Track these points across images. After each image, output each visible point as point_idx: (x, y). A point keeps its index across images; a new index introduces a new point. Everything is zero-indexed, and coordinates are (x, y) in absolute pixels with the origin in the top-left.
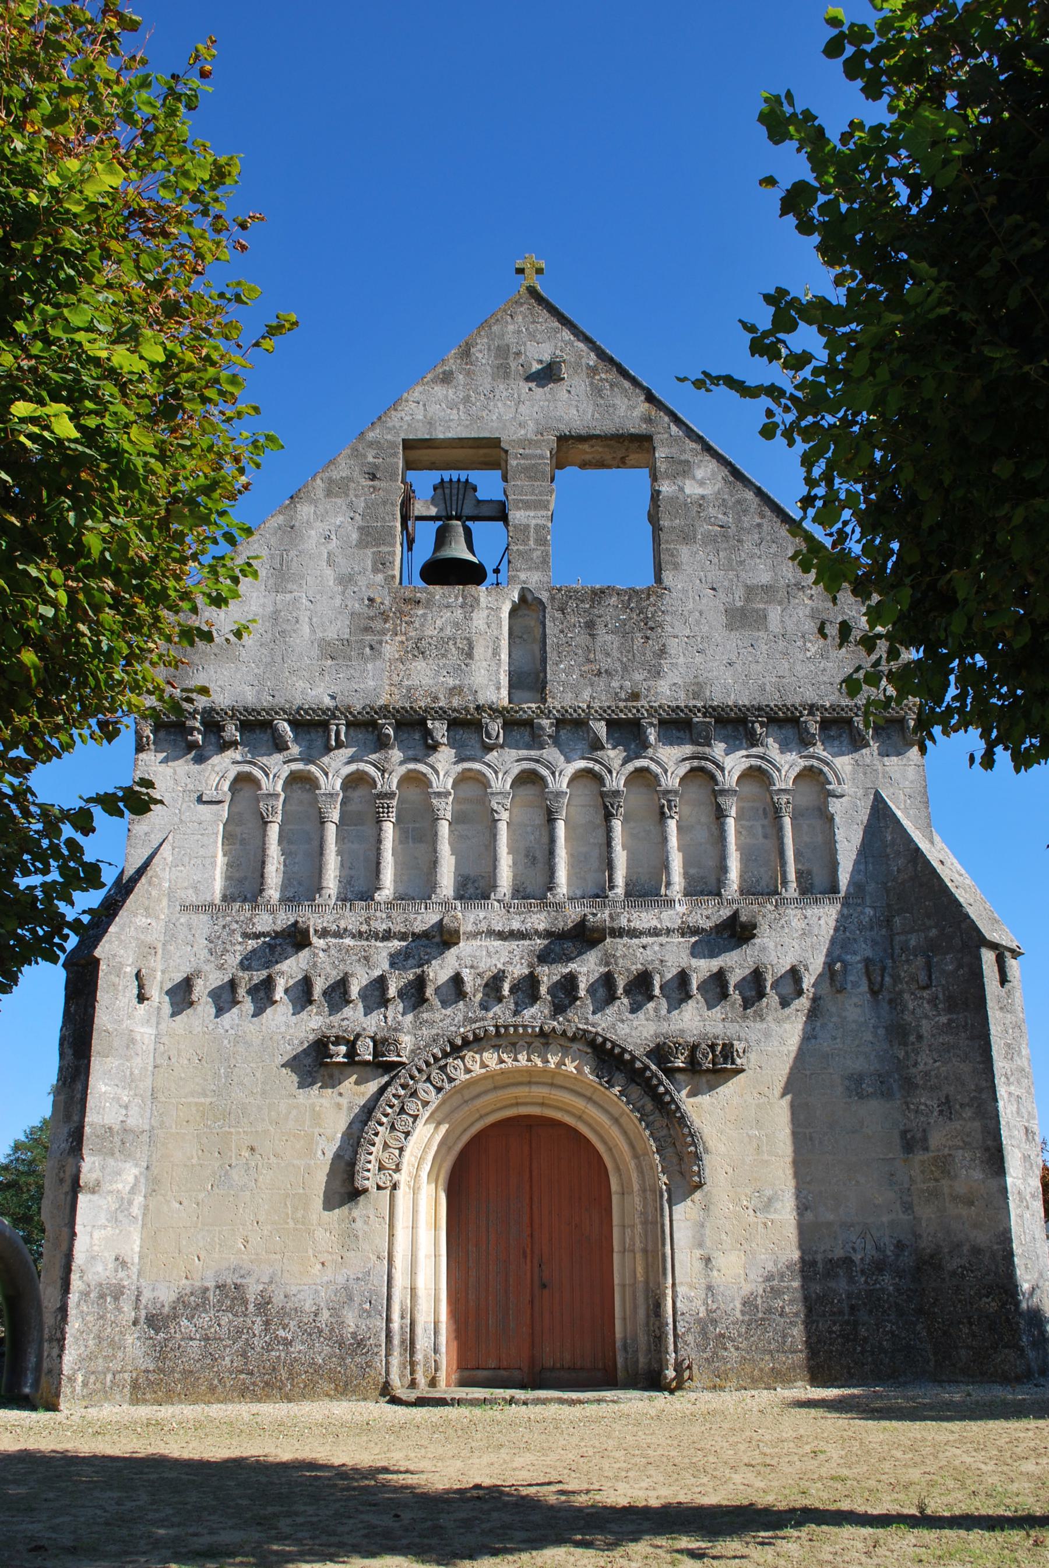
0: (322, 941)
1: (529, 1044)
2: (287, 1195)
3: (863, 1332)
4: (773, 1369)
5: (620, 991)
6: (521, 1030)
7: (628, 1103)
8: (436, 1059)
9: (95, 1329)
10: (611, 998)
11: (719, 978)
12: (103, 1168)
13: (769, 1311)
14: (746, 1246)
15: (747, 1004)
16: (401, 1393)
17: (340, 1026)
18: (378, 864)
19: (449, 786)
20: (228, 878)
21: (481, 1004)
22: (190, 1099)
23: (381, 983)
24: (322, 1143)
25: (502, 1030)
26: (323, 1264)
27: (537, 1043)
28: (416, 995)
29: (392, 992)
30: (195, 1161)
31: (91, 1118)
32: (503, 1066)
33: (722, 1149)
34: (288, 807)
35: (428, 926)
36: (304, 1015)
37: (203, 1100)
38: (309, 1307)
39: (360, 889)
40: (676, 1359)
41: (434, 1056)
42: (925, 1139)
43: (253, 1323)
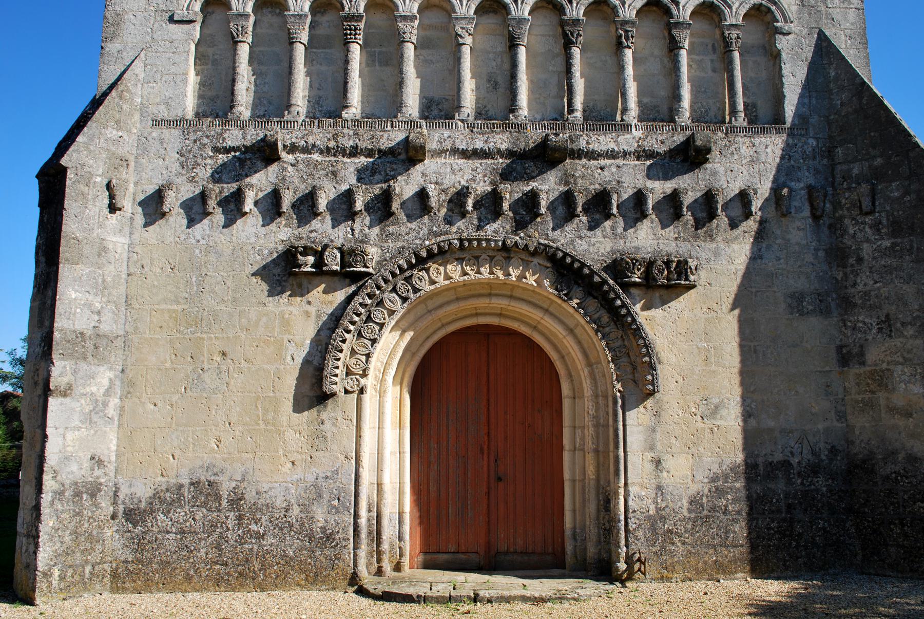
0: (290, 156)
1: (492, 258)
2: (258, 398)
3: (798, 529)
4: (716, 561)
5: (579, 209)
6: (484, 244)
7: (586, 315)
8: (402, 270)
9: (71, 526)
10: (571, 215)
11: (674, 199)
12: (75, 372)
13: (713, 509)
14: (693, 450)
15: (698, 225)
16: (367, 579)
17: (309, 238)
18: (346, 83)
19: (415, 11)
20: (201, 97)
21: (445, 219)
22: (163, 306)
23: (348, 197)
24: (292, 349)
25: (466, 244)
26: (293, 463)
27: (499, 257)
28: (382, 208)
29: (359, 205)
30: (168, 365)
31: (60, 323)
32: (466, 278)
33: (673, 360)
34: (258, 30)
35: (394, 143)
36: (273, 226)
37: (175, 307)
38: (279, 503)
39: (329, 106)
40: (627, 553)
41: (400, 267)
42: (862, 354)
43: (227, 517)
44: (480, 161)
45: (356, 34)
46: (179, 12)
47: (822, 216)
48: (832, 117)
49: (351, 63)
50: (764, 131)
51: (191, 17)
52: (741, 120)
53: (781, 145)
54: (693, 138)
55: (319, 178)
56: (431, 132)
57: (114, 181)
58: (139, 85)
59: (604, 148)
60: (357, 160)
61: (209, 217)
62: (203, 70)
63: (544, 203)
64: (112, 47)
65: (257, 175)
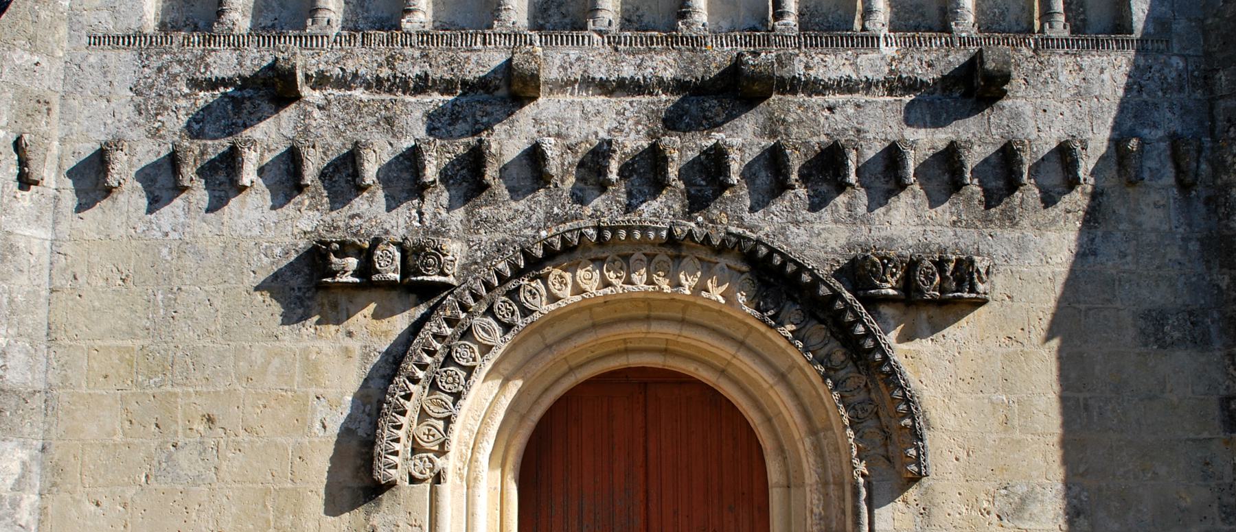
0: (317, 93)
11: (950, 158)
23: (412, 159)
29: (431, 172)
35: (487, 70)
44: (630, 99)
47: (1194, 184)
48: (1209, 21)
50: (1097, 45)
52: (1060, 28)
53: (1125, 68)
56: (549, 52)
57: (26, 137)
60: (427, 99)
61: (184, 195)
63: (735, 167)
65: (262, 125)
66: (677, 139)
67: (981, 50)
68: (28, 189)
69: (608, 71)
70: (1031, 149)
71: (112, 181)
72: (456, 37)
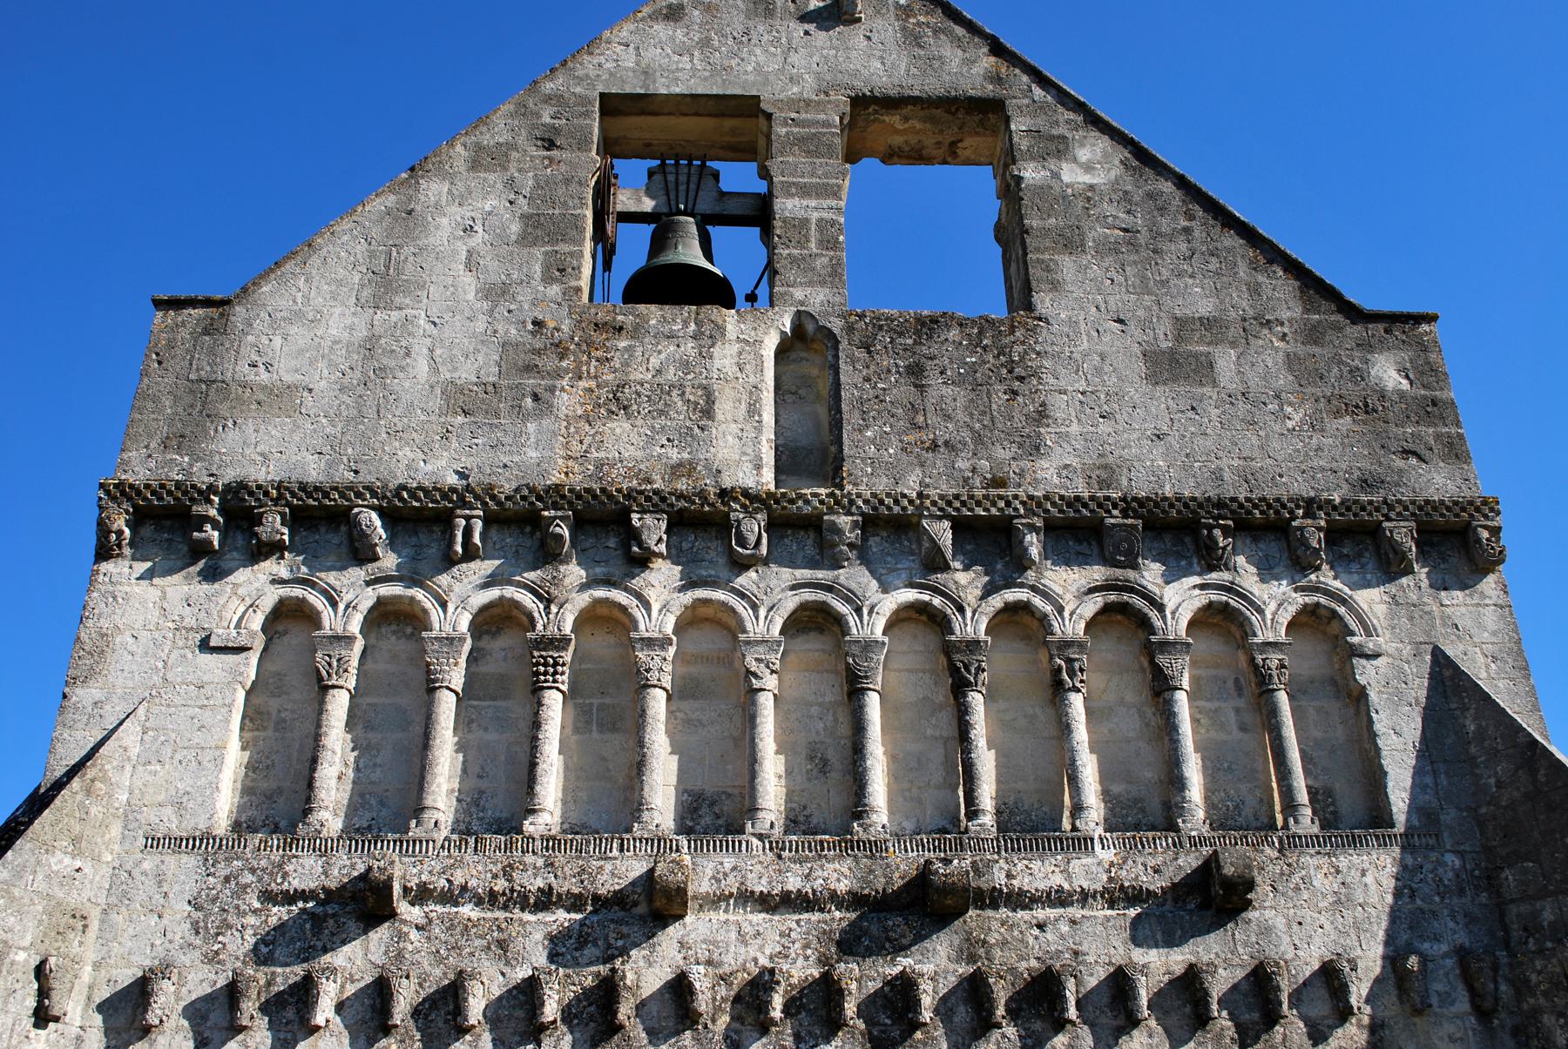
0: (416, 910)
11: (1190, 984)
18: (533, 765)
19: (669, 629)
20: (247, 791)
23: (529, 992)
29: (551, 1010)
34: (369, 666)
35: (624, 883)
39: (497, 810)
44: (796, 917)
45: (555, 673)
46: (220, 631)
47: (1494, 1010)
48: (1484, 810)
49: (545, 727)
50: (1354, 842)
51: (242, 641)
52: (1307, 823)
53: (1391, 869)
54: (1217, 861)
55: (472, 954)
56: (699, 860)
57: (52, 961)
58: (128, 768)
59: (1042, 885)
60: (549, 917)
61: (240, 1037)
62: (255, 740)
63: (927, 1001)
64: (83, 695)
65: (346, 948)
66: (855, 966)
67: (1215, 852)
68: (45, 1027)
69: (770, 883)
70: (1289, 971)
71: (152, 1018)
72: (588, 842)
